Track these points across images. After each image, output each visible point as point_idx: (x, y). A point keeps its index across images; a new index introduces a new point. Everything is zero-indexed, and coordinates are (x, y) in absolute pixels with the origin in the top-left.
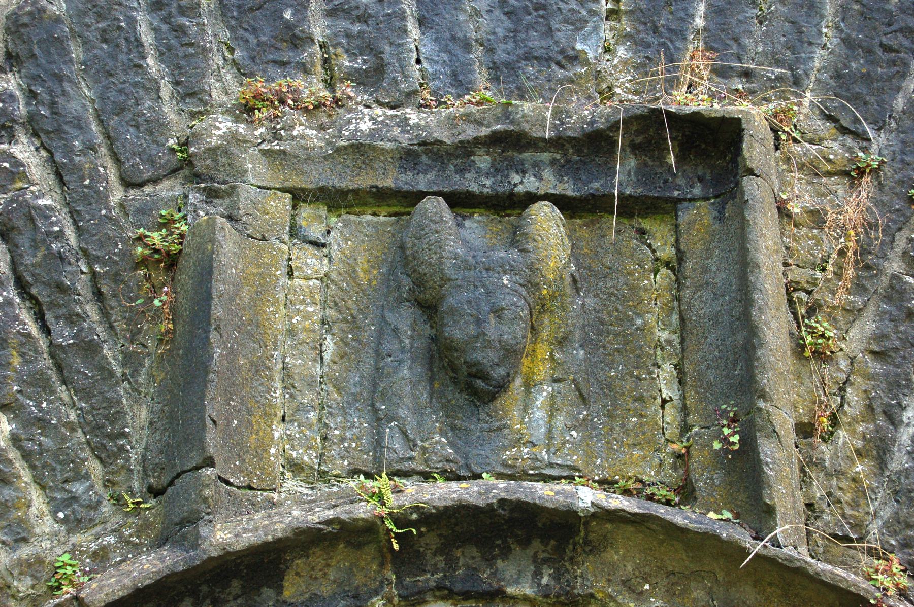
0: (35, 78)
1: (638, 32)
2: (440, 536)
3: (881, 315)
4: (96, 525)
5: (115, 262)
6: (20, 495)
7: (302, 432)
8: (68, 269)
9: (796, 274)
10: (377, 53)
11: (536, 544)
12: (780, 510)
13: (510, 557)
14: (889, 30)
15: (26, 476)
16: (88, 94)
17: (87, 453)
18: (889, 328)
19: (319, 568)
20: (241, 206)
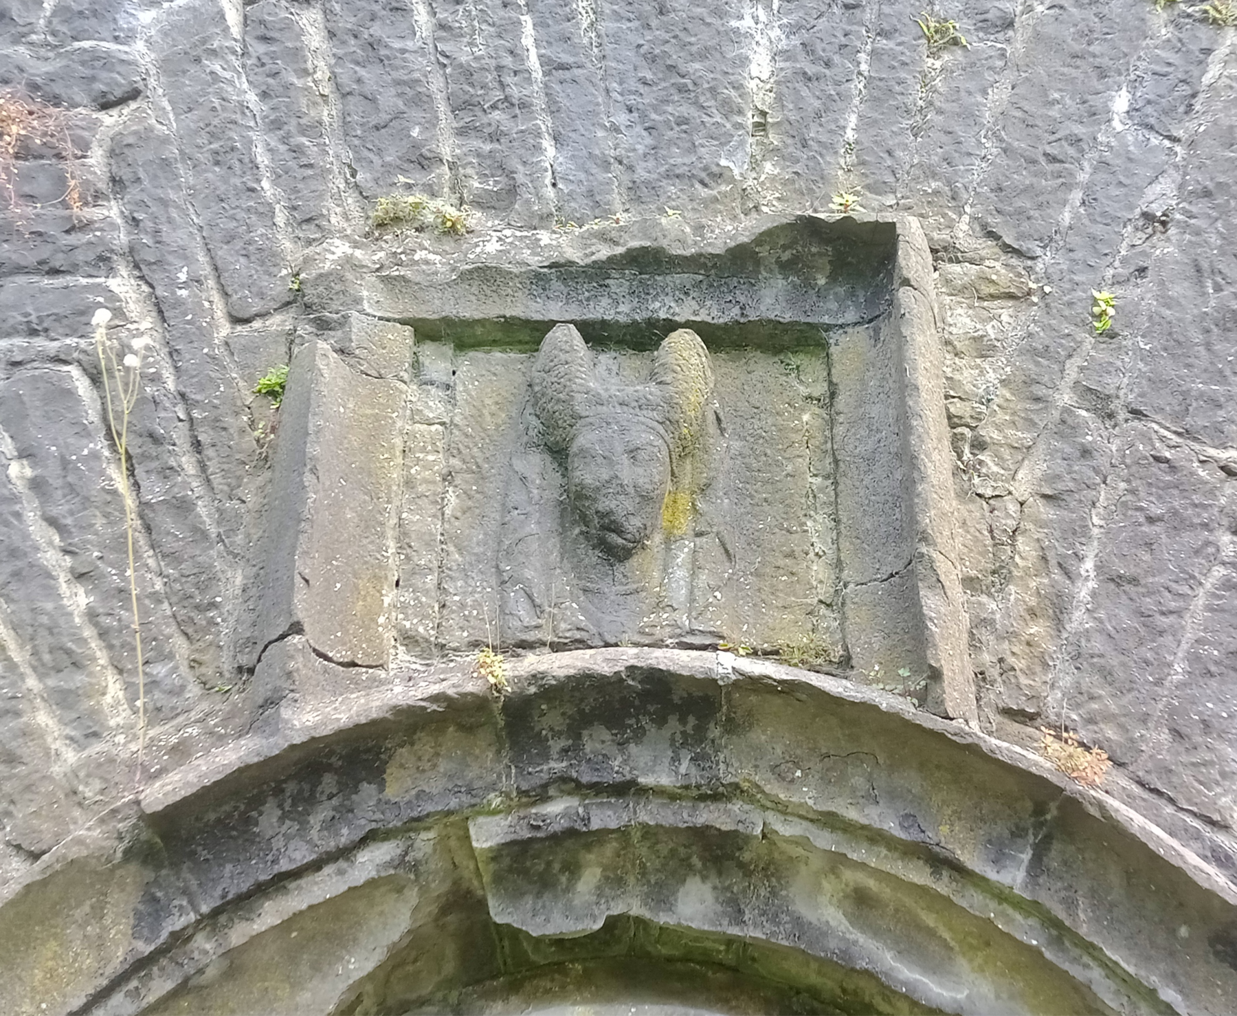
0: (142, 204)
1: (786, 146)
2: (563, 714)
3: (1052, 453)
4: (178, 715)
5: (215, 407)
6: (94, 681)
7: (417, 598)
8: (162, 414)
9: (957, 408)
10: (510, 174)
11: (673, 723)
12: (946, 673)
13: (645, 739)
14: (1053, 138)
15: (102, 658)
16: (196, 220)
17: (172, 629)
18: (1060, 466)
19: (426, 758)
20: (353, 337)
